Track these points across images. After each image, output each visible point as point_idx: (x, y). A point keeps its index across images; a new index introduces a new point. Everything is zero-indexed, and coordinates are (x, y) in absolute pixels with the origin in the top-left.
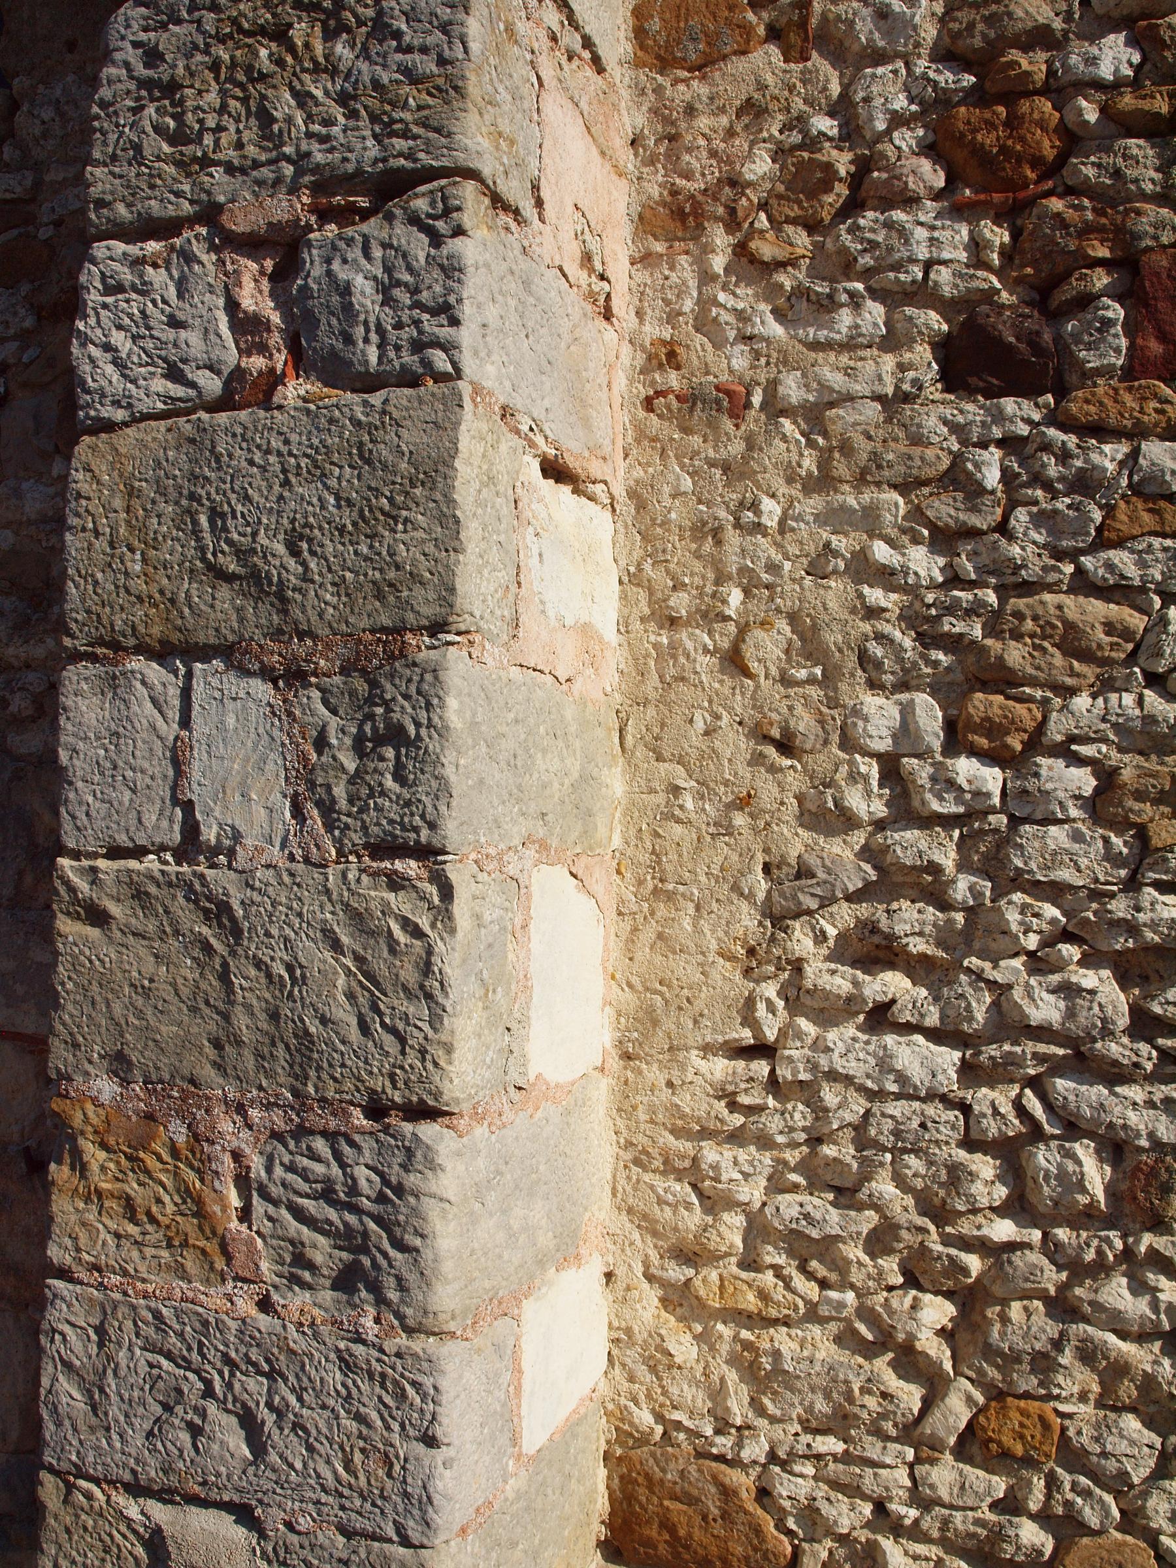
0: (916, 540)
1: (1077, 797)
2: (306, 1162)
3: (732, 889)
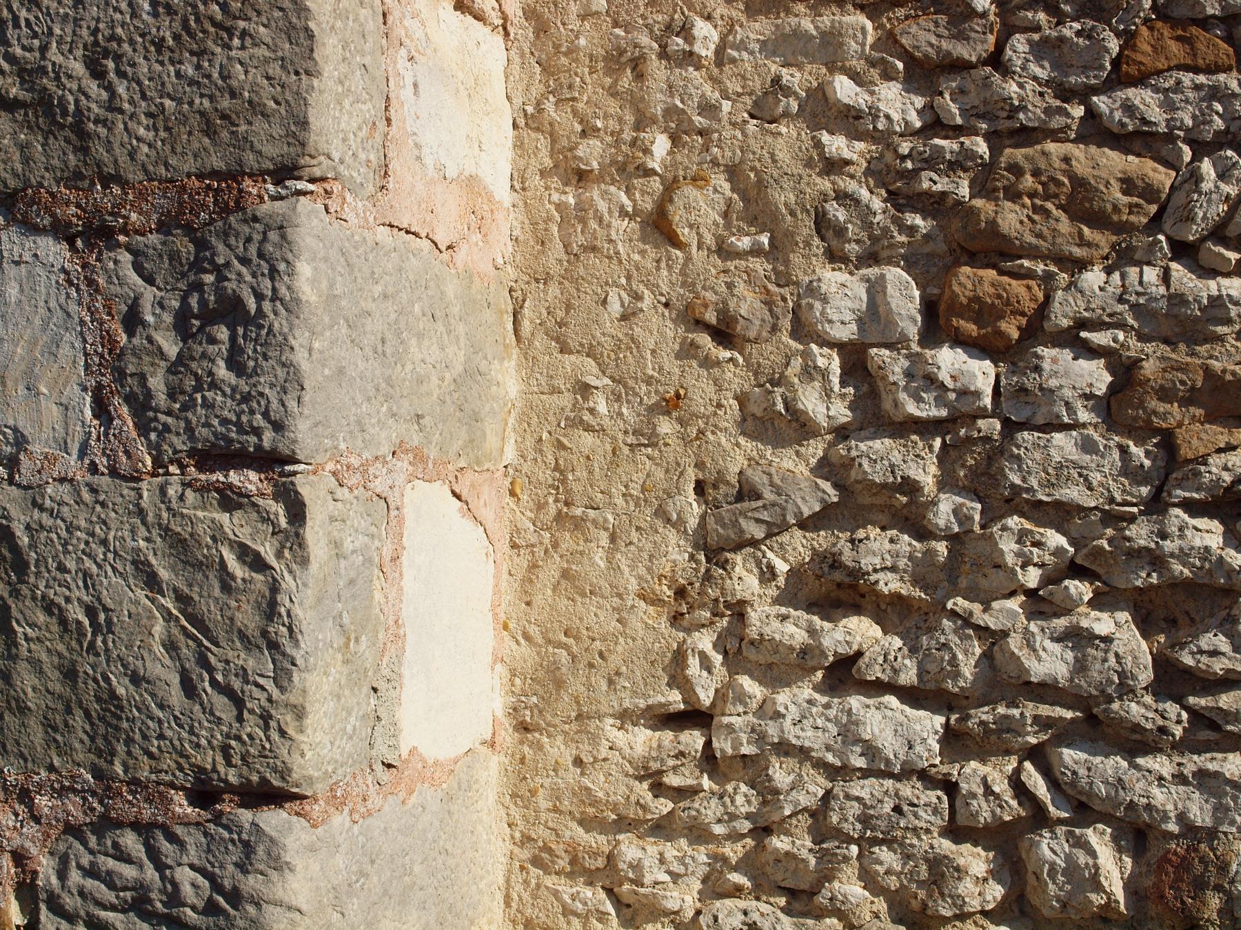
0: (888, 75)
1: (1087, 397)
2: (111, 863)
3: (656, 514)
